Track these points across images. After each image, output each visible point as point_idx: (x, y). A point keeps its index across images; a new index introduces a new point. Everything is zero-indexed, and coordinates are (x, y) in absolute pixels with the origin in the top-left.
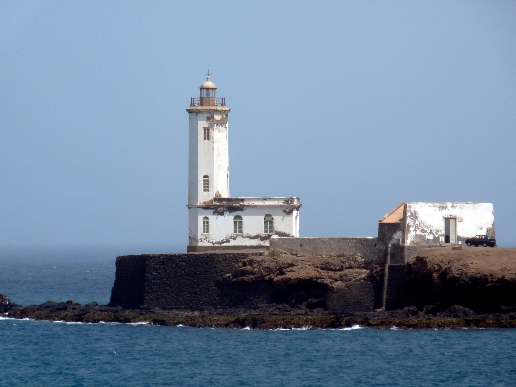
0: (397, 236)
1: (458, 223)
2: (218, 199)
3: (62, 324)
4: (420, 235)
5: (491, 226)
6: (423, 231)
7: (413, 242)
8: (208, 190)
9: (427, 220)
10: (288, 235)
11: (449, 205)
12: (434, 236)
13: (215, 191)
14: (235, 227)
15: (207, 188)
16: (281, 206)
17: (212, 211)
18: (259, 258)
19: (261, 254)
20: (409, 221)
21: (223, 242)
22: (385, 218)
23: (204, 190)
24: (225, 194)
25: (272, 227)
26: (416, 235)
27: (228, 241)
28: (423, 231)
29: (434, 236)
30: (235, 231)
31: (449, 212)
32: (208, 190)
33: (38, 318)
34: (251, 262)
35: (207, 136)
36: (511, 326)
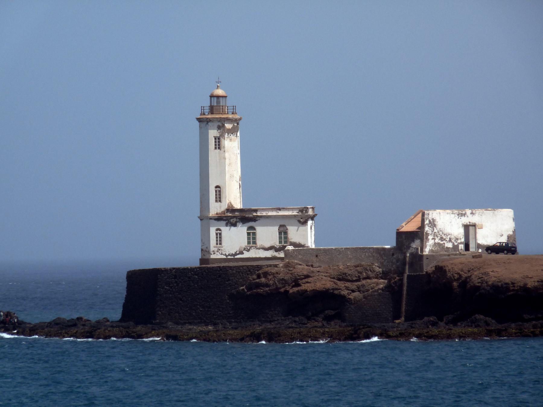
0: (416, 244)
1: (478, 231)
4: (439, 244)
5: (511, 233)
6: (442, 239)
8: (220, 201)
9: (447, 226)
10: (303, 246)
11: (468, 212)
12: (453, 244)
13: (228, 202)
14: (249, 239)
15: (219, 199)
17: (224, 223)
18: (274, 270)
19: (276, 266)
20: (427, 229)
21: (236, 254)
23: (216, 201)
25: (286, 238)
26: (435, 243)
27: (241, 253)
28: (442, 239)
29: (453, 244)
30: (249, 243)
32: (220, 201)
35: (218, 145)
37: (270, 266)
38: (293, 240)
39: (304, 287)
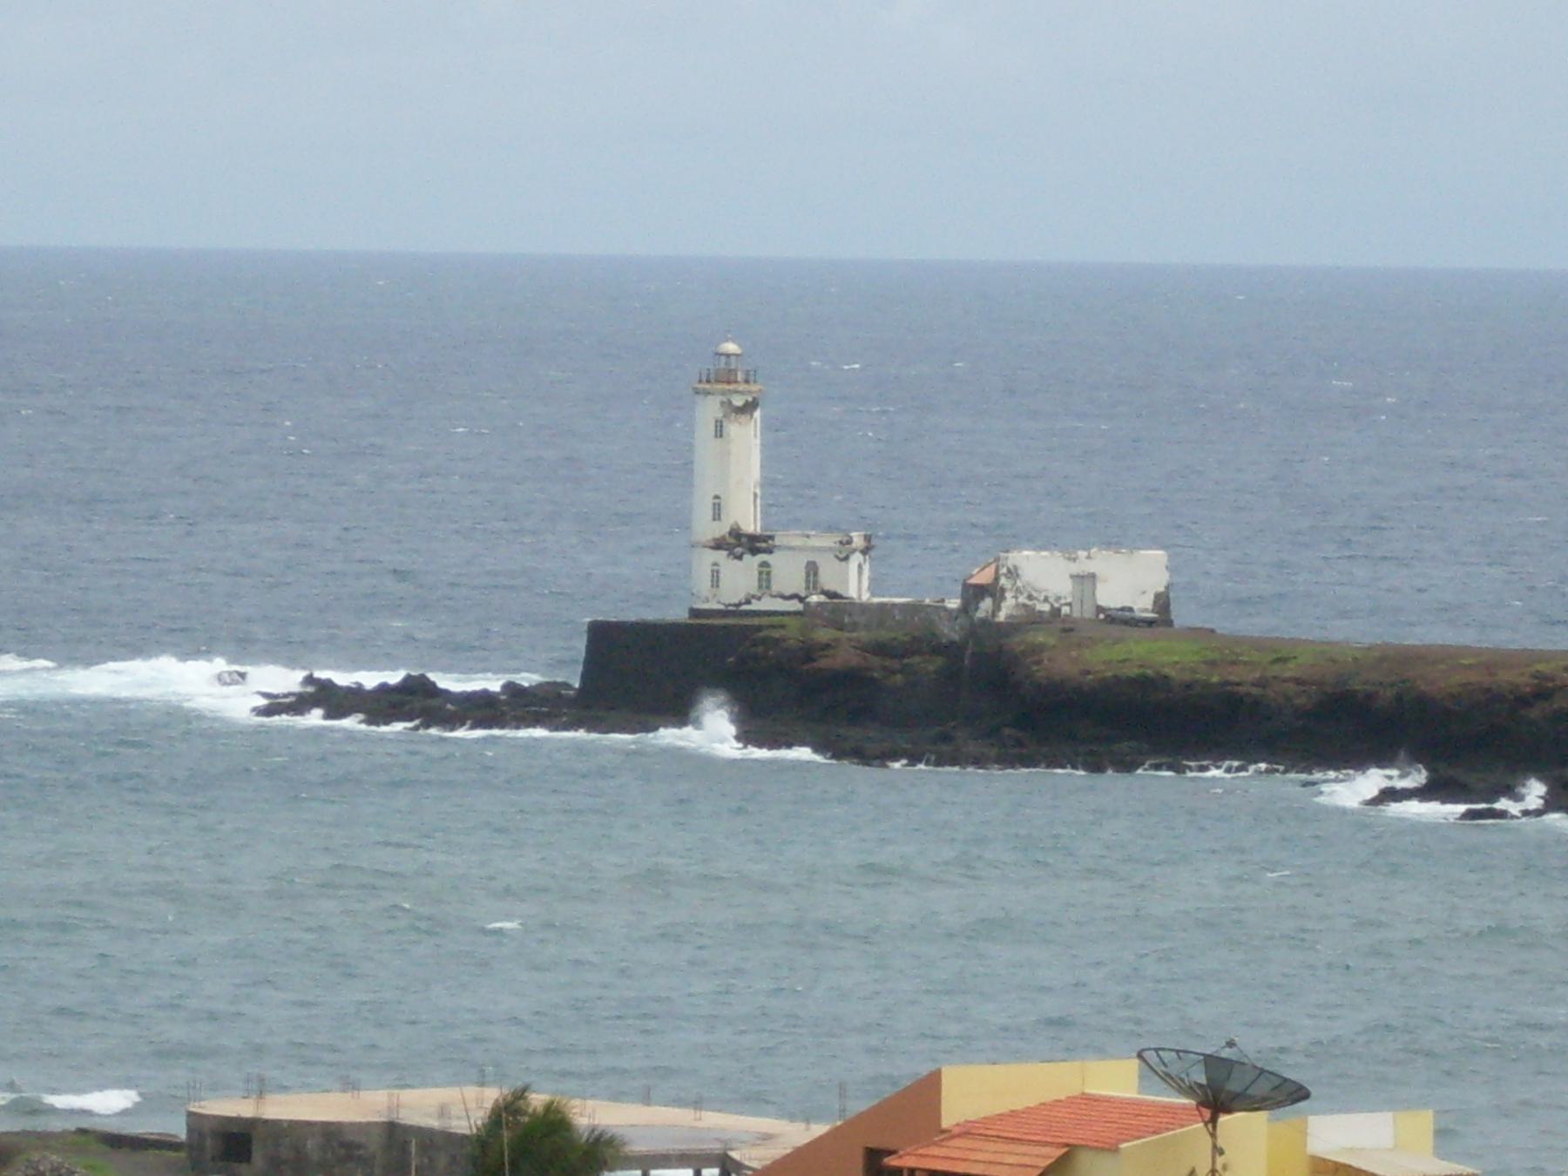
0: (987, 604)
1: (1099, 586)
2: (736, 533)
3: (485, 739)
4: (1024, 605)
5: (1161, 589)
6: (1030, 597)
7: (1008, 617)
9: (1043, 576)
10: (841, 597)
11: (1082, 554)
13: (732, 521)
14: (760, 580)
15: (717, 516)
16: (830, 549)
17: (725, 553)
18: (776, 634)
19: (783, 627)
20: (1003, 581)
21: (740, 604)
22: (972, 576)
24: (751, 526)
25: (815, 583)
26: (1017, 605)
27: (748, 602)
28: (1030, 597)
30: (760, 587)
31: (1084, 566)
33: (372, 719)
34: (764, 641)
35: (719, 432)
36: (7, 704)
37: (773, 627)
38: (826, 588)
39: (823, 663)
